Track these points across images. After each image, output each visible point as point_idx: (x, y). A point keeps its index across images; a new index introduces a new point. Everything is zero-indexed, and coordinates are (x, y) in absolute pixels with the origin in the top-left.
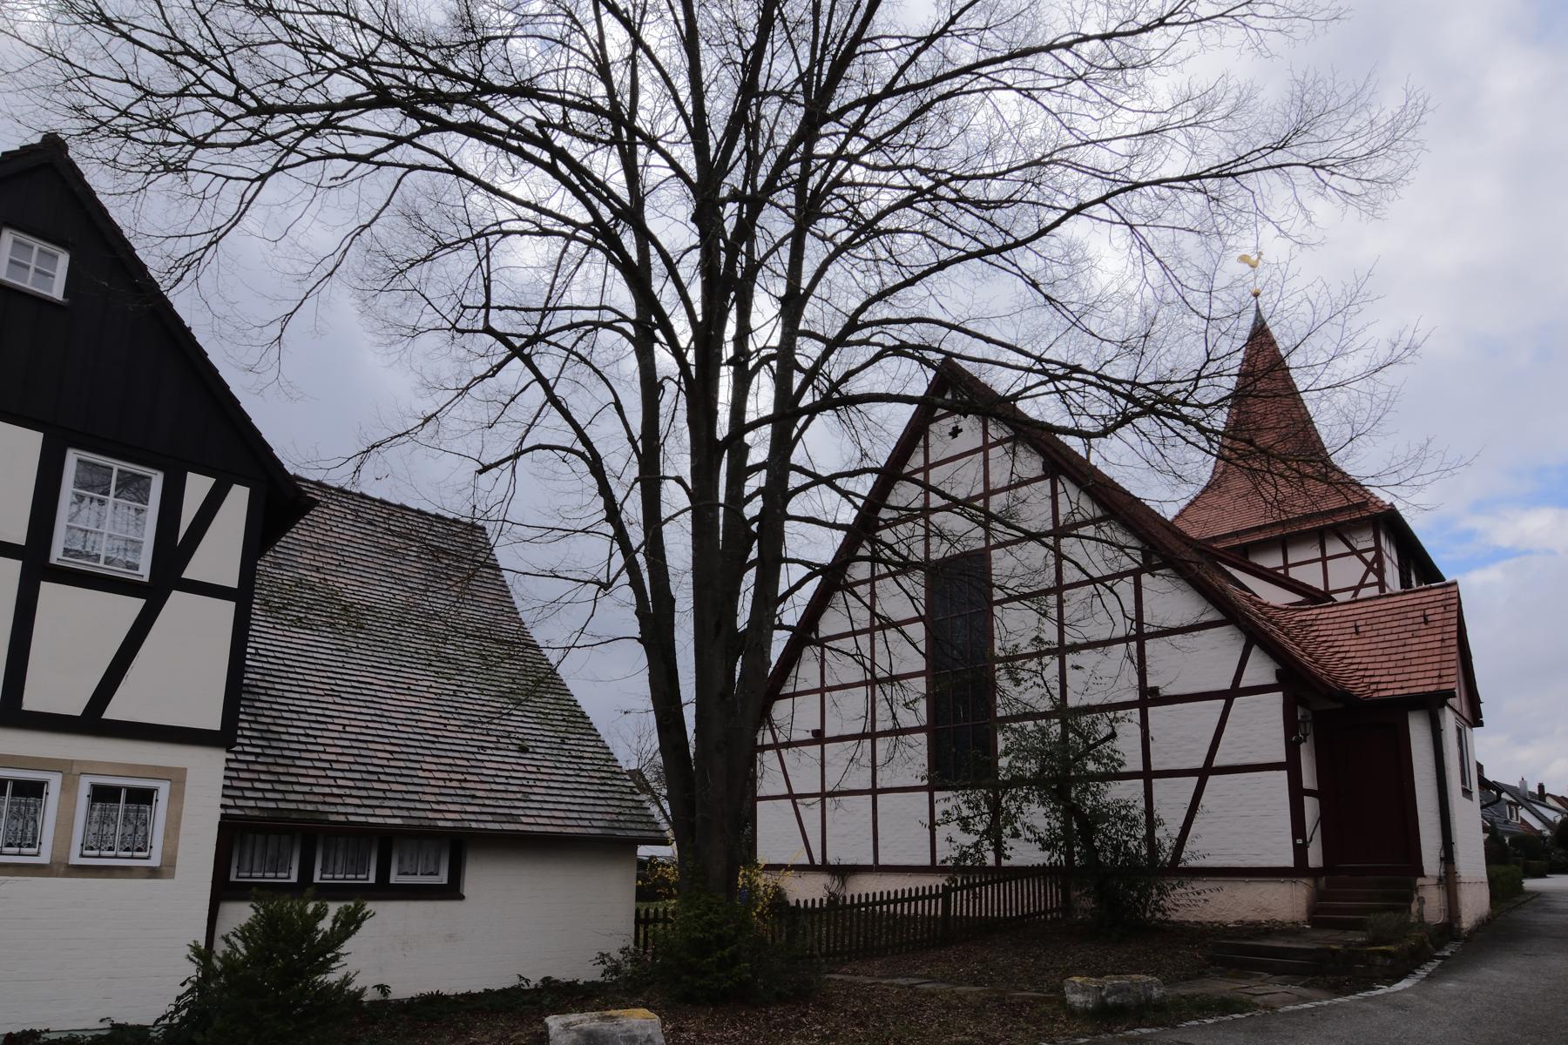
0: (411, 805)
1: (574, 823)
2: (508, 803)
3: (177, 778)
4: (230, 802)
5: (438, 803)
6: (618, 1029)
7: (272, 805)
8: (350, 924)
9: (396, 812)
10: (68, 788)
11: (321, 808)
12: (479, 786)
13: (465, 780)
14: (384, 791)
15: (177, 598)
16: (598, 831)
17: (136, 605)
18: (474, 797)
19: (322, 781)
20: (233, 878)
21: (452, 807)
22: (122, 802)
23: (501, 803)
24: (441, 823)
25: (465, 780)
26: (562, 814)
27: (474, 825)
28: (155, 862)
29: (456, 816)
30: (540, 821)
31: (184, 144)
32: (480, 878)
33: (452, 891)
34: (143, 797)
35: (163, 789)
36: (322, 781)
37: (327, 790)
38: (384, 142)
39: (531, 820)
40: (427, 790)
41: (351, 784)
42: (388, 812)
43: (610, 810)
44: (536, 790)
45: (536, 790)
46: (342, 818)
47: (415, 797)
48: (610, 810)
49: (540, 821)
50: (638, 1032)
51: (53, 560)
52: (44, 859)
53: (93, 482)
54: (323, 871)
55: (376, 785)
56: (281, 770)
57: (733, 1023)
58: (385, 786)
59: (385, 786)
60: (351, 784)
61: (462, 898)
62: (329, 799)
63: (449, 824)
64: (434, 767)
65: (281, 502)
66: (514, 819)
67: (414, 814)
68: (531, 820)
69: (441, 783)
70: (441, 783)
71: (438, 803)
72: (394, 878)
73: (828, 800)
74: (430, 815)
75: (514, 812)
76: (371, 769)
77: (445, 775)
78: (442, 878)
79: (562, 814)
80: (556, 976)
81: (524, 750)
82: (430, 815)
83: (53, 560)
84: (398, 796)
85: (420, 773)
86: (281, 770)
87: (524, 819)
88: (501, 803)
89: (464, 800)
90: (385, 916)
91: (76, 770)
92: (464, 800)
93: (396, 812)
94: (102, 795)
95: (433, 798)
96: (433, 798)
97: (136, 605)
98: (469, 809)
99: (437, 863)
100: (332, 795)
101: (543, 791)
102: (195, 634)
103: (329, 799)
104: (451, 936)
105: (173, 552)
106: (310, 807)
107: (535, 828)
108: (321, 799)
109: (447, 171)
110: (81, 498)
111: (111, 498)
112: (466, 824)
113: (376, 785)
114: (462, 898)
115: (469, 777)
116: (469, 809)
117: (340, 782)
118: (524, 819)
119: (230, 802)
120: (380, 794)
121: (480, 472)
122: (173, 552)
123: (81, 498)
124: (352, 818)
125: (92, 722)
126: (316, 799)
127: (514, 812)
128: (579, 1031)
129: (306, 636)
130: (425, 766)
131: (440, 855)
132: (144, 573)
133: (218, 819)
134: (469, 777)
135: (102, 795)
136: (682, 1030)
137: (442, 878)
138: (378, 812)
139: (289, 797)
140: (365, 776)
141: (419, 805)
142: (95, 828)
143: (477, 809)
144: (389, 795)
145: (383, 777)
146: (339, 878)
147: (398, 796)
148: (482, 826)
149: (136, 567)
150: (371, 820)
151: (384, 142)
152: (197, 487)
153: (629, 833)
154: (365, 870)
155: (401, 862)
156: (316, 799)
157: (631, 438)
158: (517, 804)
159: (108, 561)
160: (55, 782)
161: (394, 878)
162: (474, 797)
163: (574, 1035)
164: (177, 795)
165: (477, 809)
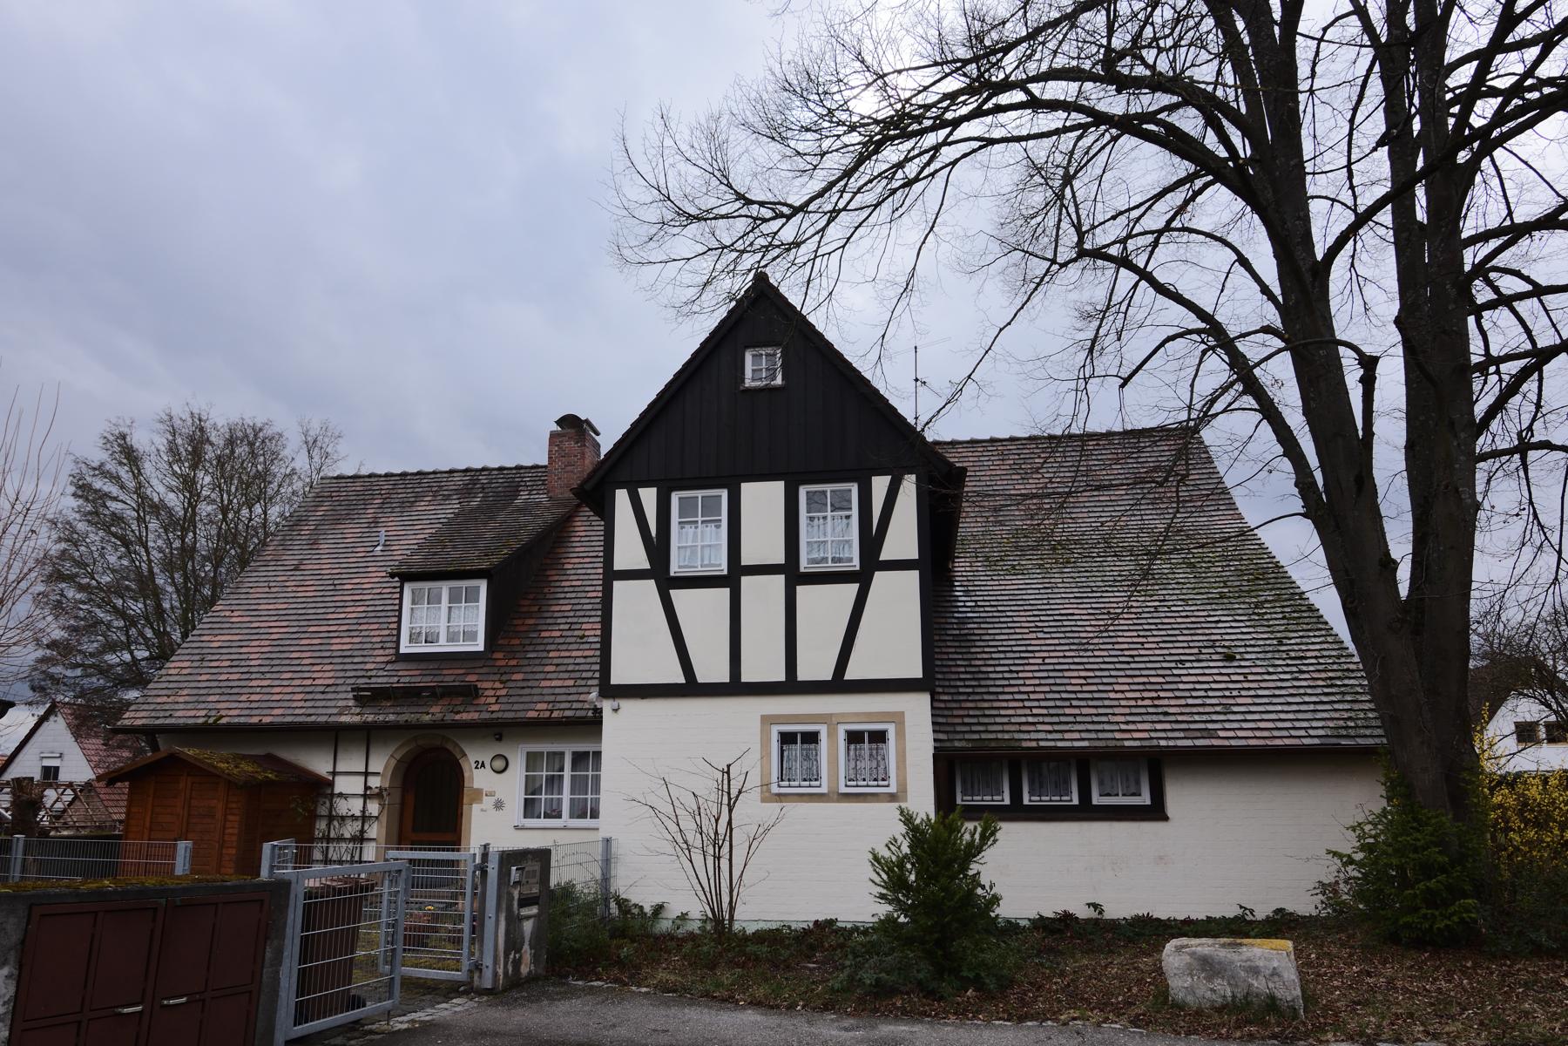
0: (1100, 727)
1: (1285, 733)
2: (1204, 718)
3: (898, 718)
4: (942, 736)
5: (1127, 723)
6: (1235, 957)
7: (976, 736)
8: (988, 836)
9: (1084, 735)
10: (832, 734)
11: (1016, 736)
12: (1173, 702)
13: (1159, 698)
14: (1075, 715)
15: (879, 576)
16: (1316, 741)
17: (853, 588)
18: (1166, 714)
19: (1020, 712)
20: (1026, 802)
21: (1140, 726)
22: (865, 740)
23: (1197, 718)
24: (1127, 743)
25: (1159, 698)
26: (1270, 725)
27: (1163, 743)
28: (893, 789)
29: (1146, 735)
30: (1240, 734)
31: (1084, 127)
32: (1181, 797)
33: (1156, 811)
34: (879, 737)
35: (891, 730)
36: (1020, 712)
37: (1023, 719)
38: (951, 139)
39: (1231, 734)
40: (1117, 711)
41: (1044, 711)
42: (1077, 736)
43: (1337, 715)
44: (1240, 701)
45: (1240, 701)
46: (1034, 744)
47: (1104, 719)
48: (1337, 715)
49: (1240, 734)
50: (1261, 963)
51: (802, 570)
52: (824, 790)
53: (816, 502)
54: (1031, 793)
55: (1068, 711)
56: (986, 705)
57: (1450, 973)
58: (1077, 711)
59: (1077, 711)
60: (1044, 711)
61: (1166, 819)
62: (1024, 728)
63: (1137, 743)
64: (1126, 687)
65: (942, 476)
66: (1211, 734)
67: (1101, 735)
68: (1231, 734)
69: (1133, 703)
70: (1133, 703)
71: (1127, 723)
72: (1097, 800)
73: (675, 569)
74: (1118, 735)
75: (1210, 726)
76: (1064, 696)
77: (1137, 695)
78: (1145, 799)
79: (1270, 725)
80: (1290, 908)
81: (1230, 658)
82: (1118, 735)
83: (802, 570)
84: (1088, 719)
85: (1112, 695)
86: (986, 705)
87: (1221, 734)
88: (1197, 718)
89: (1155, 718)
90: (1011, 834)
91: (834, 720)
92: (1155, 718)
93: (1084, 735)
94: (854, 738)
95: (1122, 719)
96: (1122, 719)
97: (853, 588)
98: (1159, 726)
99: (1138, 783)
100: (1027, 723)
101: (1249, 701)
102: (897, 599)
103: (1024, 728)
104: (1161, 858)
105: (871, 541)
106: (1007, 736)
107: (1233, 743)
108: (1016, 728)
109: (981, 148)
110: (812, 519)
111: (829, 514)
112: (1155, 743)
113: (1068, 711)
114: (1166, 819)
115: (1162, 694)
116: (1159, 726)
117: (1035, 711)
118: (1221, 734)
119: (942, 736)
120: (1071, 719)
121: (1122, 386)
122: (871, 541)
123: (812, 519)
124: (1042, 744)
125: (839, 684)
126: (1013, 728)
127: (1210, 726)
128: (1192, 954)
129: (1019, 581)
130: (1117, 688)
131: (1122, 778)
132: (856, 564)
133: (932, 751)
134: (1162, 694)
135: (854, 738)
136: (1369, 974)
137: (1145, 799)
138: (1067, 736)
139: (991, 728)
140: (1059, 703)
141: (1107, 727)
142: (852, 764)
143: (1168, 726)
144: (1079, 719)
145: (1075, 703)
146: (1046, 800)
147: (1088, 719)
148: (1171, 743)
149: (850, 560)
150: (1060, 744)
151: (951, 139)
152: (880, 484)
153: (1360, 741)
154: (1068, 792)
155: (1101, 783)
156: (1013, 728)
157: (1265, 290)
158: (1214, 717)
159: (834, 560)
160: (823, 730)
161: (1097, 800)
162: (1166, 714)
163: (1187, 958)
164: (901, 734)
165: (1168, 726)
